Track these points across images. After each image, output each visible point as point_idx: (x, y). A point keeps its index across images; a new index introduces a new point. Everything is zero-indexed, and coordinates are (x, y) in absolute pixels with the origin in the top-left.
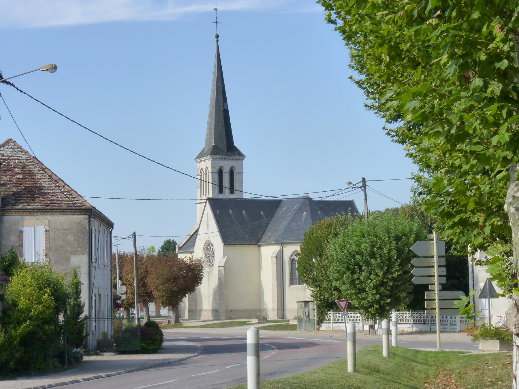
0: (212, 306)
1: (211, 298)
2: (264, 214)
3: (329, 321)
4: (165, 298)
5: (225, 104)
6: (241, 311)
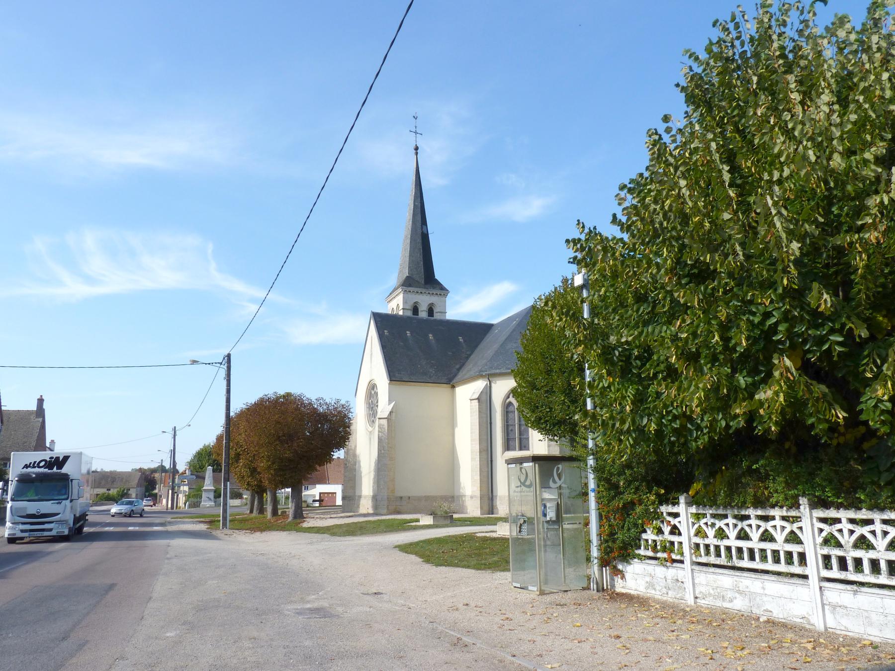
2: (465, 341)
3: (668, 554)
6: (419, 499)
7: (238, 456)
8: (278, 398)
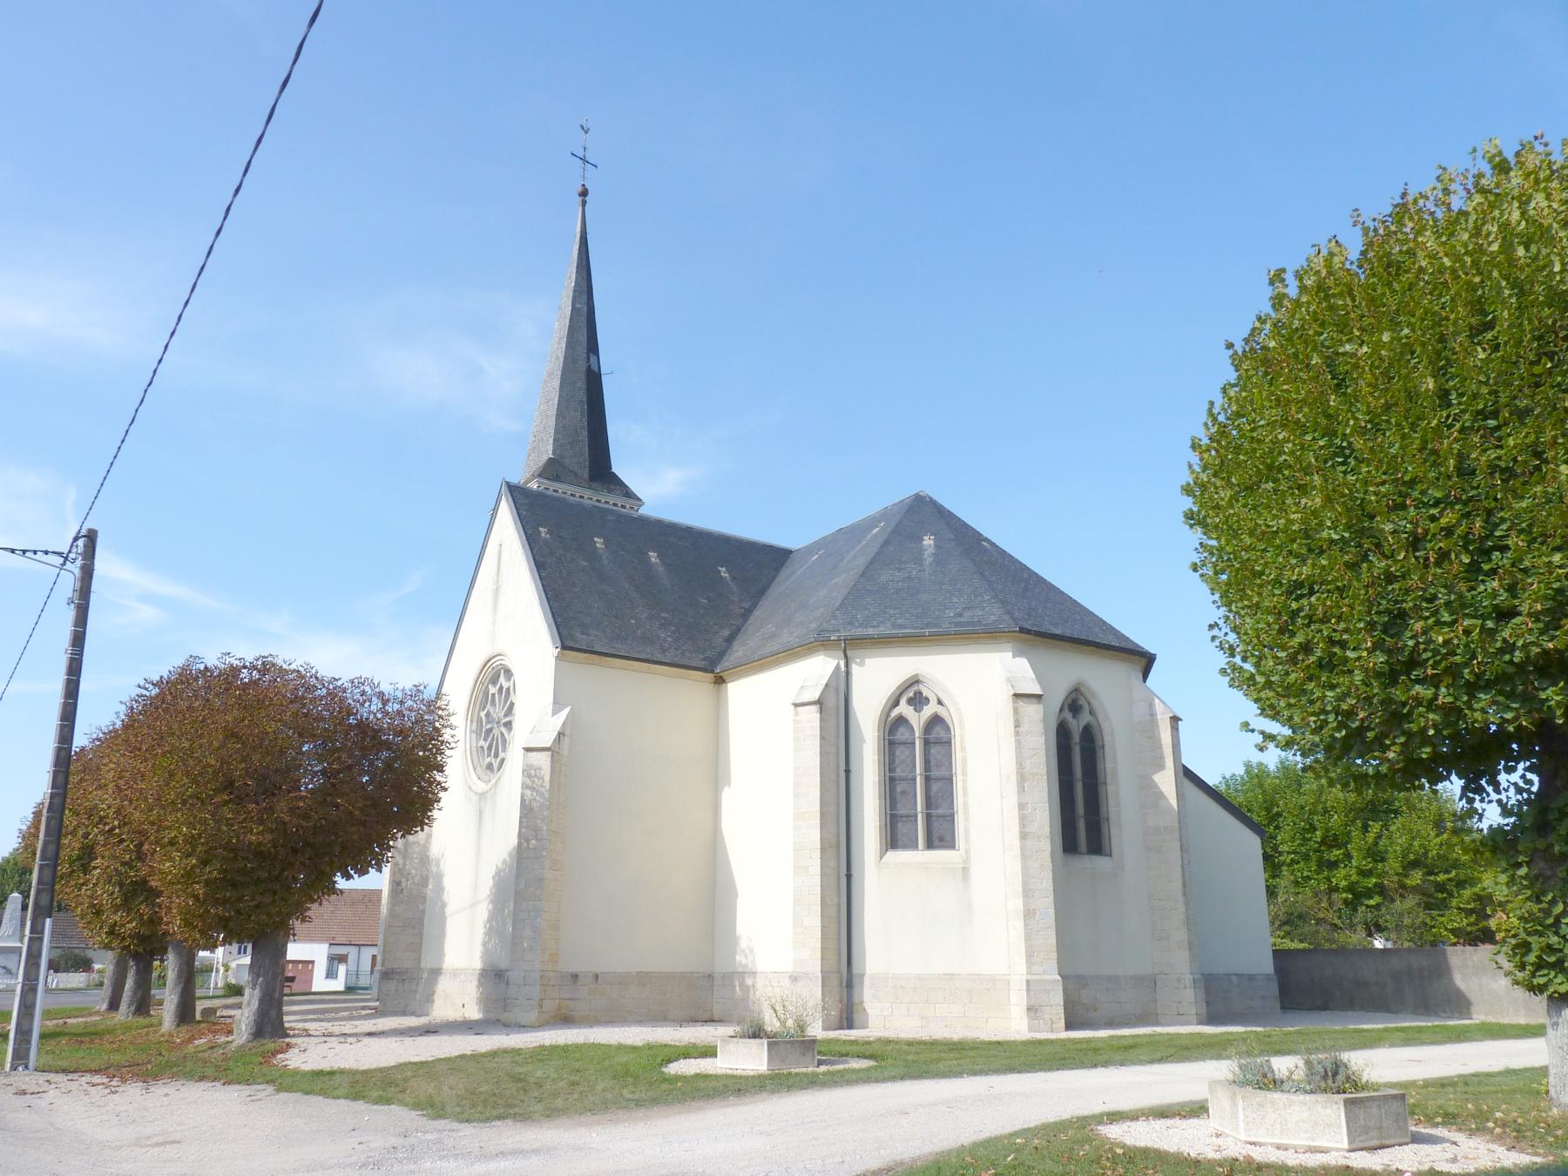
0: (486, 953)
1: (483, 912)
2: (734, 578)
4: (199, 889)
5: (593, 359)
6: (623, 980)
7: (87, 854)
8: (234, 671)
